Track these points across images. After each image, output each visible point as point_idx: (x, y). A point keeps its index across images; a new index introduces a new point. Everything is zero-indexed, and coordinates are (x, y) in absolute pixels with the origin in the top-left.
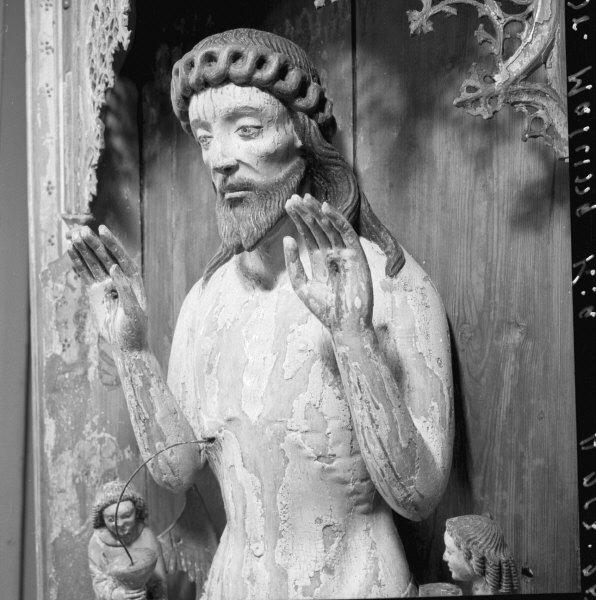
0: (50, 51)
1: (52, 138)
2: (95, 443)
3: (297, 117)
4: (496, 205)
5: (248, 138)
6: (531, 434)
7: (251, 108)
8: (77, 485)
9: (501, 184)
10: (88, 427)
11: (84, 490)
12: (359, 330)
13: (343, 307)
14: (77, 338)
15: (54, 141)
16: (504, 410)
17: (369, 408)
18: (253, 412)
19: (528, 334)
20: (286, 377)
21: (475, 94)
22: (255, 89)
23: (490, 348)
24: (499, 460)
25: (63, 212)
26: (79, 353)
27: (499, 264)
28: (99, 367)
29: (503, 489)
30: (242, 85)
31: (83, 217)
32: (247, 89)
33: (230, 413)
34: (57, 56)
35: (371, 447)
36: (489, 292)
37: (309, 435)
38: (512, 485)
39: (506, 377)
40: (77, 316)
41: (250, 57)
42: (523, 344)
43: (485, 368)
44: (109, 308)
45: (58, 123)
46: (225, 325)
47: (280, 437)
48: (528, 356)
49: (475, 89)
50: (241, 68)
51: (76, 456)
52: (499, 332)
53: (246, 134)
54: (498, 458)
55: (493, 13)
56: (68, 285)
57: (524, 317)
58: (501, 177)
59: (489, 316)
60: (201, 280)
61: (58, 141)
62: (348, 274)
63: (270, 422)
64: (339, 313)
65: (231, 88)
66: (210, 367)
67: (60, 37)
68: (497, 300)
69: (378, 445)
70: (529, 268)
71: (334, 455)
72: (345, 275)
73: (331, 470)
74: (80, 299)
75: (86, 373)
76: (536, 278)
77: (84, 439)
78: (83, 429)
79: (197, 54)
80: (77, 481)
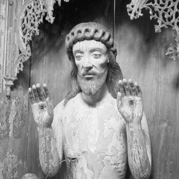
0: (3, 19)
1: (2, 49)
2: (10, 159)
3: (110, 53)
4: (160, 85)
5: (97, 58)
6: (169, 154)
7: (99, 49)
8: (3, 174)
9: (162, 79)
10: (8, 153)
11: (6, 176)
12: (138, 124)
13: (134, 116)
14: (6, 121)
15: (3, 51)
16: (161, 147)
17: (138, 148)
18: (93, 150)
19: (169, 124)
20: (105, 138)
21: (172, 52)
22: (101, 42)
23: (157, 128)
24: (159, 162)
25: (4, 76)
26: (7, 126)
27: (160, 103)
28: (13, 132)
29: (160, 171)
30: (97, 41)
31: (14, 79)
32: (98, 42)
33: (84, 150)
34: (6, 21)
35: (136, 160)
36: (157, 111)
37: (112, 157)
38: (163, 170)
39: (162, 136)
40: (7, 113)
41: (92, 31)
42: (167, 127)
43: (155, 134)
44: (40, 113)
45: (5, 45)
46: (79, 119)
47: (102, 158)
48: (169, 131)
49: (172, 51)
50: (98, 35)
51: (3, 164)
52: (160, 123)
53: (96, 57)
54: (158, 162)
55: (177, 29)
56: (4, 102)
57: (168, 119)
58: (162, 77)
59: (157, 118)
60: (63, 101)
61: (4, 50)
62: (137, 105)
63: (99, 153)
64: (133, 118)
65: (93, 41)
66: (75, 134)
67: (7, 15)
68: (159, 113)
69: (139, 160)
70: (170, 104)
71: (119, 163)
72: (136, 106)
73: (118, 168)
74: (8, 107)
75: (8, 133)
76: (172, 108)
77: (7, 157)
78: (7, 154)
79: (75, 30)
80: (3, 173)
